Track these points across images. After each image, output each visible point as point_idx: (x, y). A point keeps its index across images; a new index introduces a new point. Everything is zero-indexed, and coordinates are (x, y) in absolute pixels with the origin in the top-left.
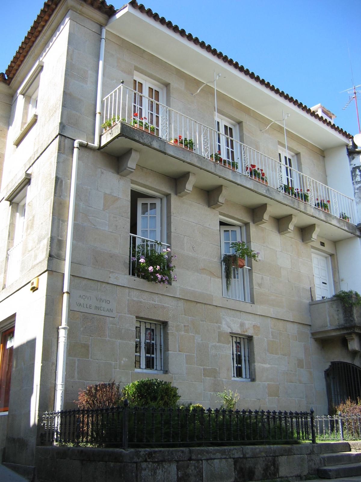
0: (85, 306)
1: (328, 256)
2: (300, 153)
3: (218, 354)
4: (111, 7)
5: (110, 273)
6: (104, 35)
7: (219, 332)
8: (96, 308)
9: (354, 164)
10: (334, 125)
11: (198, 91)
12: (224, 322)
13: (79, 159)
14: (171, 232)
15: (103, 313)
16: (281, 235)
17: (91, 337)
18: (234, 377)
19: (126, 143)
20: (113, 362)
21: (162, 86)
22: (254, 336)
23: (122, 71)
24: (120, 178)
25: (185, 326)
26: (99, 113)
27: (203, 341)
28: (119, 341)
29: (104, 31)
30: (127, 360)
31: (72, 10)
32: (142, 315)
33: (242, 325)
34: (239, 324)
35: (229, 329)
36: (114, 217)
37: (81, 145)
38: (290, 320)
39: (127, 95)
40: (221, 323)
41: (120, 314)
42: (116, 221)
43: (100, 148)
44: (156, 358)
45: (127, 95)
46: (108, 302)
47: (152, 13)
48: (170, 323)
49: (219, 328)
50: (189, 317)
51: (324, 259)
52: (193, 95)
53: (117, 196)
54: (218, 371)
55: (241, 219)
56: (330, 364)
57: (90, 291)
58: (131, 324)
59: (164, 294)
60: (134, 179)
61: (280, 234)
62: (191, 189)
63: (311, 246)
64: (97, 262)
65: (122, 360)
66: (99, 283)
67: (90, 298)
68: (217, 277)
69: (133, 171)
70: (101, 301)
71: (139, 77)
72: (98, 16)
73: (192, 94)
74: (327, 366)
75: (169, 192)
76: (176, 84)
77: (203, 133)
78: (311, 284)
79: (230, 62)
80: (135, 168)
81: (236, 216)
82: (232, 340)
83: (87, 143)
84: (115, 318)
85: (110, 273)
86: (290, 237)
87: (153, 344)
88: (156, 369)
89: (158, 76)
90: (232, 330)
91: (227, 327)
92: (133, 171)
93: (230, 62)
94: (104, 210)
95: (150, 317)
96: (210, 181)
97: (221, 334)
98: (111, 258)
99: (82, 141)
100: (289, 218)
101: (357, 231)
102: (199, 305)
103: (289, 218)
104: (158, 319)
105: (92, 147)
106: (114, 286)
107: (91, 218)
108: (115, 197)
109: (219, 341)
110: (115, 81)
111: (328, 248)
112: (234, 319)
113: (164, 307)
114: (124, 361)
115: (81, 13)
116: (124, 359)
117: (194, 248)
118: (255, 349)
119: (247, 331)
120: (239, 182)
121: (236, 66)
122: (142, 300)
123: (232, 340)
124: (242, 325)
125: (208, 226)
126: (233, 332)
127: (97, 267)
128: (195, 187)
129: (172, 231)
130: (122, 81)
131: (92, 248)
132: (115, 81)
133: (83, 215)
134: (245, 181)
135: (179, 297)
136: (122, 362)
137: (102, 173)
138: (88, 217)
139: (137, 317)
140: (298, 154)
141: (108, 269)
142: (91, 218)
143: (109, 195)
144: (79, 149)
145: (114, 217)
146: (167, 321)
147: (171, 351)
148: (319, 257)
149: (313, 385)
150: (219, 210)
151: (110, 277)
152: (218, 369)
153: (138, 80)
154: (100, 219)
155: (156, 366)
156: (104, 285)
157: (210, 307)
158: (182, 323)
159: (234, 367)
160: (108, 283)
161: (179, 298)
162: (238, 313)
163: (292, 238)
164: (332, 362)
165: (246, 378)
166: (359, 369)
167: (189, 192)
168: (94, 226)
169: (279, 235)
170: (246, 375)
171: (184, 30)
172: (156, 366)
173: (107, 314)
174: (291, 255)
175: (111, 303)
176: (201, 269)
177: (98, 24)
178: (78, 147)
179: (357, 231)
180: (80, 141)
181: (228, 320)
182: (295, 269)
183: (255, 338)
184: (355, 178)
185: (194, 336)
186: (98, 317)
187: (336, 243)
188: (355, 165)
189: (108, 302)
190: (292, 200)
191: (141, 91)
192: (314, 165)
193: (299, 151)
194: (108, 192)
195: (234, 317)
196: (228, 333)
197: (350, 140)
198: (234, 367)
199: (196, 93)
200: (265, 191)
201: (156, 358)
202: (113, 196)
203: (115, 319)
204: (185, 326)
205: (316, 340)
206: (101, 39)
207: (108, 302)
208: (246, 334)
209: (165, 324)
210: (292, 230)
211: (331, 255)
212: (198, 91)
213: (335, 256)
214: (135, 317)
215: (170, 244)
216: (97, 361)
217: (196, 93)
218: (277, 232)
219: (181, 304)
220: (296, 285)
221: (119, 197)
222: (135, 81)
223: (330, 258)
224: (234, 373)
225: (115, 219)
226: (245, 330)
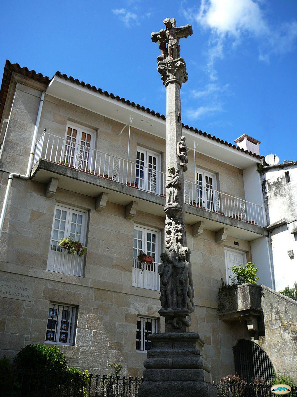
0: (5, 292)
1: (244, 253)
2: (218, 173)
3: (124, 331)
4: (47, 78)
5: (30, 268)
6: (43, 99)
7: (126, 314)
8: (15, 294)
9: (264, 178)
10: (247, 151)
11: (121, 132)
12: (132, 306)
13: (12, 185)
14: (88, 237)
15: (21, 298)
16: (194, 238)
17: (7, 316)
18: (143, 350)
19: (45, 174)
20: (25, 336)
21: (93, 130)
23: (57, 122)
24: (47, 199)
25: (94, 309)
26: (32, 153)
27: (110, 321)
28: (32, 319)
29: (43, 95)
30: (38, 334)
31: (19, 83)
32: (56, 300)
33: (150, 309)
34: (147, 308)
35: (137, 311)
36: (38, 227)
37: (14, 176)
38: (198, 305)
39: (48, 141)
40: (129, 307)
42: (40, 230)
43: (30, 178)
44: (56, 332)
45: (48, 141)
46: (25, 289)
47: (73, 79)
49: (127, 310)
50: (99, 302)
51: (241, 256)
52: (119, 135)
53: (43, 212)
54: (123, 344)
55: (156, 226)
56: (236, 341)
57: (11, 281)
58: (46, 307)
59: (71, 283)
60: (58, 199)
61: (193, 237)
62: (105, 205)
63: (224, 245)
64: (20, 260)
65: (33, 334)
66: (20, 276)
67: (10, 286)
68: (128, 271)
69: (55, 193)
70: (20, 289)
71: (74, 126)
72: (40, 86)
73: (118, 135)
74: (235, 343)
75: (89, 208)
76: (102, 128)
77: (114, 162)
78: (222, 275)
79: (143, 109)
80: (55, 191)
81: (151, 224)
82: (144, 321)
83: (19, 175)
84: (30, 302)
85: (30, 268)
86: (203, 239)
87: (146, 340)
88: (55, 341)
89: (87, 123)
90: (139, 312)
91: (135, 310)
92: (55, 193)
93: (143, 109)
94: (30, 222)
95: (62, 302)
96: (123, 198)
97: (127, 316)
98: (32, 257)
99: (15, 174)
100: (198, 224)
101: (265, 232)
102: (109, 292)
103: (198, 224)
104: (70, 303)
105: (24, 178)
106: (33, 278)
107: (18, 228)
108: (41, 212)
109: (126, 321)
110: (50, 130)
111: (241, 246)
112: (142, 304)
113: (75, 294)
114: (35, 335)
115: (26, 85)
116: (35, 333)
118: (161, 328)
119: (154, 314)
120: (144, 198)
121: (148, 111)
122: (56, 288)
123: (144, 321)
124: (150, 309)
125: (123, 233)
126: (141, 314)
127: (19, 264)
128: (108, 203)
129: (89, 237)
130: (45, 129)
131: (17, 250)
132: (50, 130)
133: (12, 226)
134: (150, 197)
135: (90, 286)
136: (34, 335)
137: (32, 196)
138: (16, 228)
139: (50, 301)
140: (217, 174)
141: (28, 266)
142: (18, 228)
143: (36, 211)
144: (13, 180)
145: (38, 227)
146: (78, 304)
148: (235, 254)
149: (220, 359)
150: (134, 220)
151: (29, 271)
152: (123, 343)
153: (141, 152)
154: (26, 229)
155: (55, 338)
156: (24, 277)
158: (92, 306)
159: (143, 342)
160: (28, 276)
161: (90, 287)
162: (146, 299)
163: (205, 239)
164: (238, 340)
165: (70, 342)
166: (258, 347)
167: (103, 207)
168: (20, 234)
169: (192, 237)
170: (70, 340)
171: (101, 90)
172: (55, 338)
173: (24, 298)
174: (203, 253)
175: (28, 291)
176: (113, 265)
177: (39, 90)
178: (12, 178)
179: (265, 232)
180: (14, 174)
181: (136, 304)
182: (206, 264)
184: (265, 190)
185: (102, 317)
186: (16, 301)
187: (250, 243)
188: (264, 179)
189: (26, 290)
190: (196, 210)
191: (143, 159)
192: (232, 181)
193: (217, 171)
194: (34, 209)
195: (142, 302)
196: (136, 315)
197: (262, 159)
198: (143, 342)
199: (120, 134)
201: (56, 332)
202: (39, 212)
203: (31, 302)
204: (94, 309)
205: (224, 321)
206: (40, 101)
207: (25, 289)
208: (153, 316)
209: (77, 307)
210: (202, 233)
211: (247, 252)
212: (121, 132)
213: (249, 253)
214: (49, 301)
215: (87, 246)
216: (11, 334)
217: (120, 134)
218: (190, 235)
219: (92, 292)
220: (206, 277)
221: (45, 213)
222: (138, 153)
223: (245, 254)
224: (143, 348)
225: (39, 229)
226: (152, 312)
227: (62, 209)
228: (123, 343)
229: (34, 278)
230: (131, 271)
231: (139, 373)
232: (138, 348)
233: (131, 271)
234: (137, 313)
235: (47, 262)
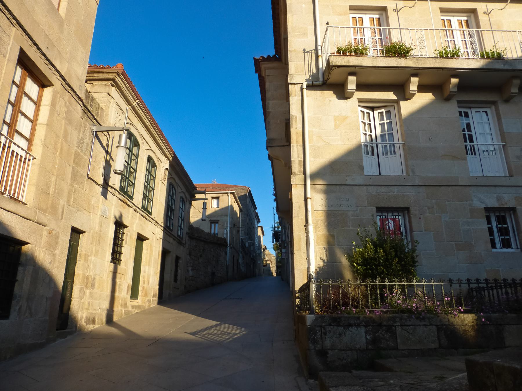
22: (517, 208)
41: (360, 208)
48: (412, 208)
117: (431, 139)
119: (506, 204)
124: (499, 199)
137: (330, 101)
147: (414, 232)
157: (456, 188)
183: (519, 208)
186: (340, 212)
200: (502, 65)
204: (428, 208)
209: (407, 209)
219: (422, 189)
227: (357, 16)
228: (473, 243)
229: (365, 187)
230: (465, 159)
231: (501, 275)
232: (494, 246)
233: (466, 159)
234: (483, 206)
235: (363, 167)
